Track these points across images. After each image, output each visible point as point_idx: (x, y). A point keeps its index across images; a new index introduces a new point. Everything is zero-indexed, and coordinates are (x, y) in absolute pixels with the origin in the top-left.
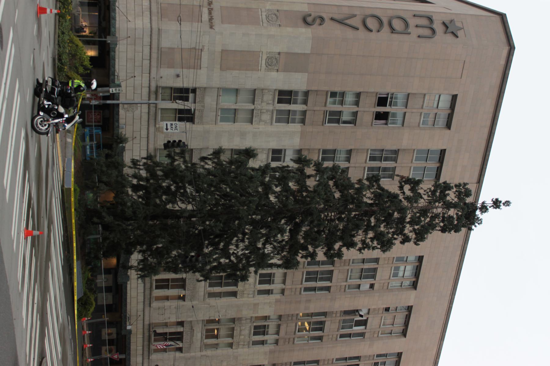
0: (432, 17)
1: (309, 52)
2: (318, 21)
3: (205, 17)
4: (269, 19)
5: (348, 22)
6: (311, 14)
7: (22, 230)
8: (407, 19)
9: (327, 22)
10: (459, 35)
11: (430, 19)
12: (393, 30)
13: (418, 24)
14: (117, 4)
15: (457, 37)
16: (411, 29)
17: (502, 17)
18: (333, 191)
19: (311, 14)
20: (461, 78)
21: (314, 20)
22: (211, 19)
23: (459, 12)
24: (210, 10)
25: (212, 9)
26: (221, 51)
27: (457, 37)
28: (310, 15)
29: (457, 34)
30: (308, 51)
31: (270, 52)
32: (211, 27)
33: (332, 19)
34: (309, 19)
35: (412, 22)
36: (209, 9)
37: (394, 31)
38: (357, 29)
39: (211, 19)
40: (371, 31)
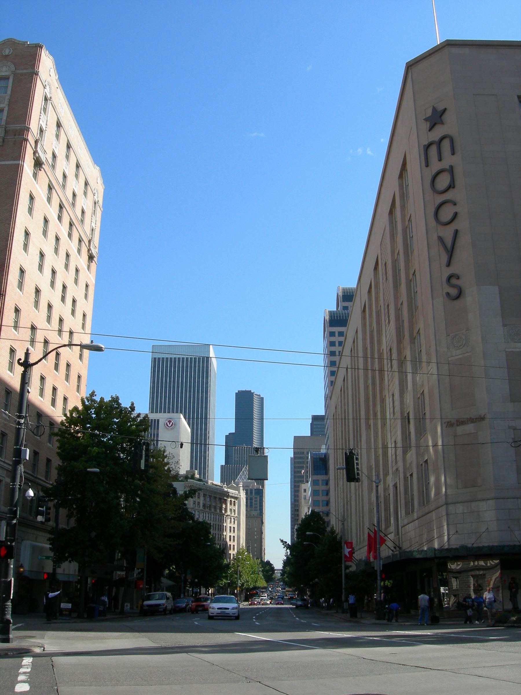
0: (425, 145)
1: (497, 288)
2: (454, 281)
3: (470, 428)
4: (461, 345)
5: (449, 244)
6: (446, 293)
7: (404, 632)
8: (433, 175)
9: (454, 269)
10: (443, 108)
11: (427, 147)
12: (451, 186)
13: (437, 160)
14: (470, 545)
15: (445, 110)
16: (445, 164)
17: (410, 66)
18: (194, 589)
19: (446, 293)
20: (496, 95)
21: (453, 286)
22: (472, 420)
23: (414, 118)
24: (458, 424)
25: (458, 421)
26: (512, 403)
27: (445, 110)
28: (448, 294)
29: (442, 110)
30: (496, 289)
31: (505, 338)
32: (482, 419)
33: (448, 265)
34: (454, 292)
35: (436, 166)
36: (457, 425)
37: (452, 186)
38: (456, 232)
39: (472, 420)
40: (456, 215)
